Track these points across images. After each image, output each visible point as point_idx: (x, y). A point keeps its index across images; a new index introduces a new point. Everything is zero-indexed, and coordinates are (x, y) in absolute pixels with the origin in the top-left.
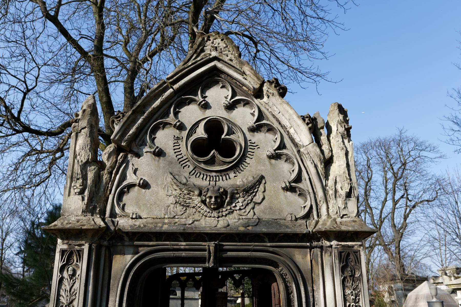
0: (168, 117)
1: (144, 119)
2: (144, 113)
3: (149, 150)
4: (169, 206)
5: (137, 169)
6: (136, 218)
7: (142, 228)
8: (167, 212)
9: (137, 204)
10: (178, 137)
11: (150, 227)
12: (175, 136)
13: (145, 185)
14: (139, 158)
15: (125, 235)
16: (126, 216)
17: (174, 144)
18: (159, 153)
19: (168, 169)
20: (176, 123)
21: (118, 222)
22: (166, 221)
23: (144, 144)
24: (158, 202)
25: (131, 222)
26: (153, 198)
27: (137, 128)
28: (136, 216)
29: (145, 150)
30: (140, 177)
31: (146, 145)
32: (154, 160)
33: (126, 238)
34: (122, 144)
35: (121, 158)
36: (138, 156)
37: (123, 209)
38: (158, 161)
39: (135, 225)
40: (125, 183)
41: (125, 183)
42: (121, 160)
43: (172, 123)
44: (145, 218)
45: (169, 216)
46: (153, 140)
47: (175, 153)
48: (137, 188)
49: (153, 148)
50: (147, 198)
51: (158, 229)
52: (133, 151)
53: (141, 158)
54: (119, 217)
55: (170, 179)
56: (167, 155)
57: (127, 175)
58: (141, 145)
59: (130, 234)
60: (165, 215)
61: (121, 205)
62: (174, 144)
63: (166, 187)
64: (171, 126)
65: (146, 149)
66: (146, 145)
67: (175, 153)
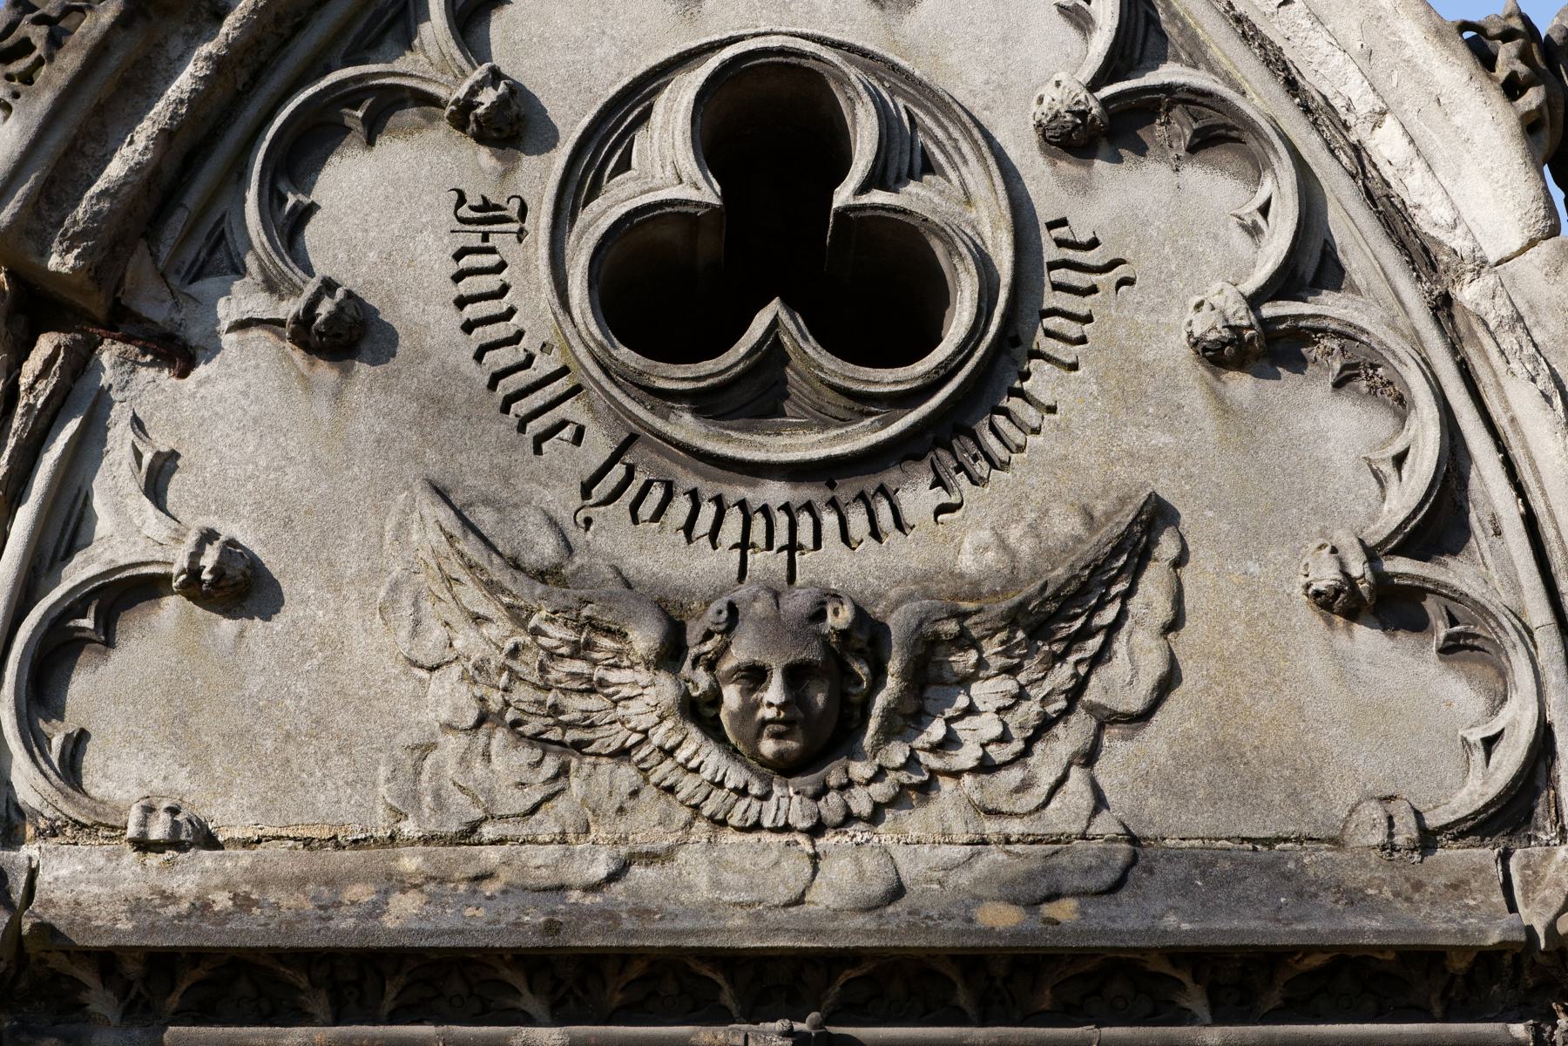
0: (407, 41)
1: (219, 64)
2: (219, 17)
3: (257, 304)
4: (427, 748)
5: (174, 455)
6: (174, 843)
7: (226, 916)
8: (416, 798)
9: (180, 731)
10: (486, 205)
11: (287, 914)
12: (462, 200)
13: (239, 587)
14: (183, 374)
15: (87, 976)
16: (97, 826)
17: (458, 256)
18: (343, 334)
19: (416, 457)
20: (474, 91)
21: (33, 873)
22: (410, 862)
23: (220, 257)
24: (343, 719)
25: (134, 874)
26: (300, 687)
27: (166, 137)
28: (176, 826)
29: (228, 310)
30: (195, 525)
31: (239, 271)
32: (307, 384)
33: (100, 1001)
34: (53, 262)
35: (44, 373)
36: (179, 354)
37: (70, 769)
38: (337, 395)
39: (169, 898)
40: (79, 571)
41: (79, 571)
42: (45, 388)
43: (441, 92)
44: (247, 843)
45: (431, 827)
46: (290, 228)
47: (468, 327)
48: (172, 606)
49: (296, 290)
50: (254, 684)
51: (344, 927)
52: (139, 319)
53: (201, 371)
54: (40, 833)
55: (435, 537)
56: (404, 343)
57: (98, 503)
58: (198, 272)
59: (133, 969)
60: (399, 815)
61: (57, 742)
62: (458, 256)
63: (406, 602)
64: (431, 119)
65: (241, 300)
66: (239, 271)
67: (468, 327)
